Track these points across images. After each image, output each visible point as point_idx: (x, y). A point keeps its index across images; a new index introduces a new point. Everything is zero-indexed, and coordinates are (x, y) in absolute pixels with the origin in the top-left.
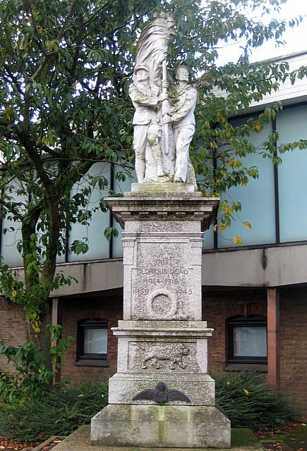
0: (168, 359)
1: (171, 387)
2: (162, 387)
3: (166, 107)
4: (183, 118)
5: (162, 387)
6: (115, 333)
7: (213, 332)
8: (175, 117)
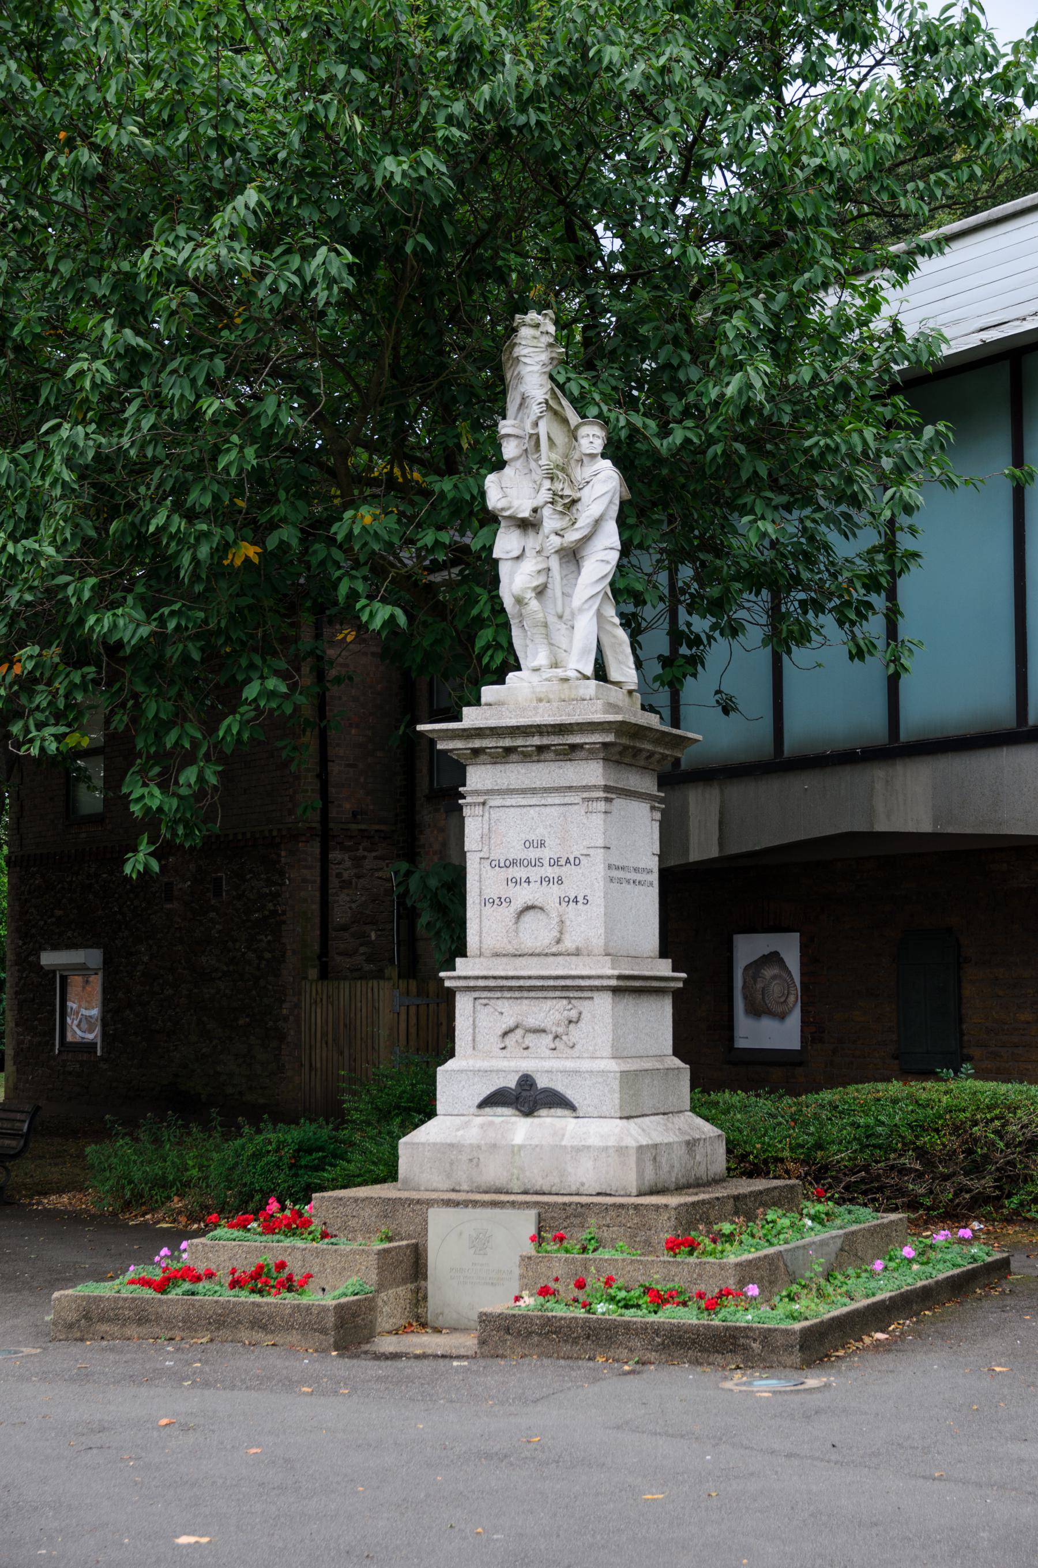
0: (544, 1031)
1: (542, 1083)
2: (526, 1081)
3: (550, 521)
4: (587, 539)
5: (526, 1081)
6: (448, 984)
7: (685, 981)
8: (573, 536)
